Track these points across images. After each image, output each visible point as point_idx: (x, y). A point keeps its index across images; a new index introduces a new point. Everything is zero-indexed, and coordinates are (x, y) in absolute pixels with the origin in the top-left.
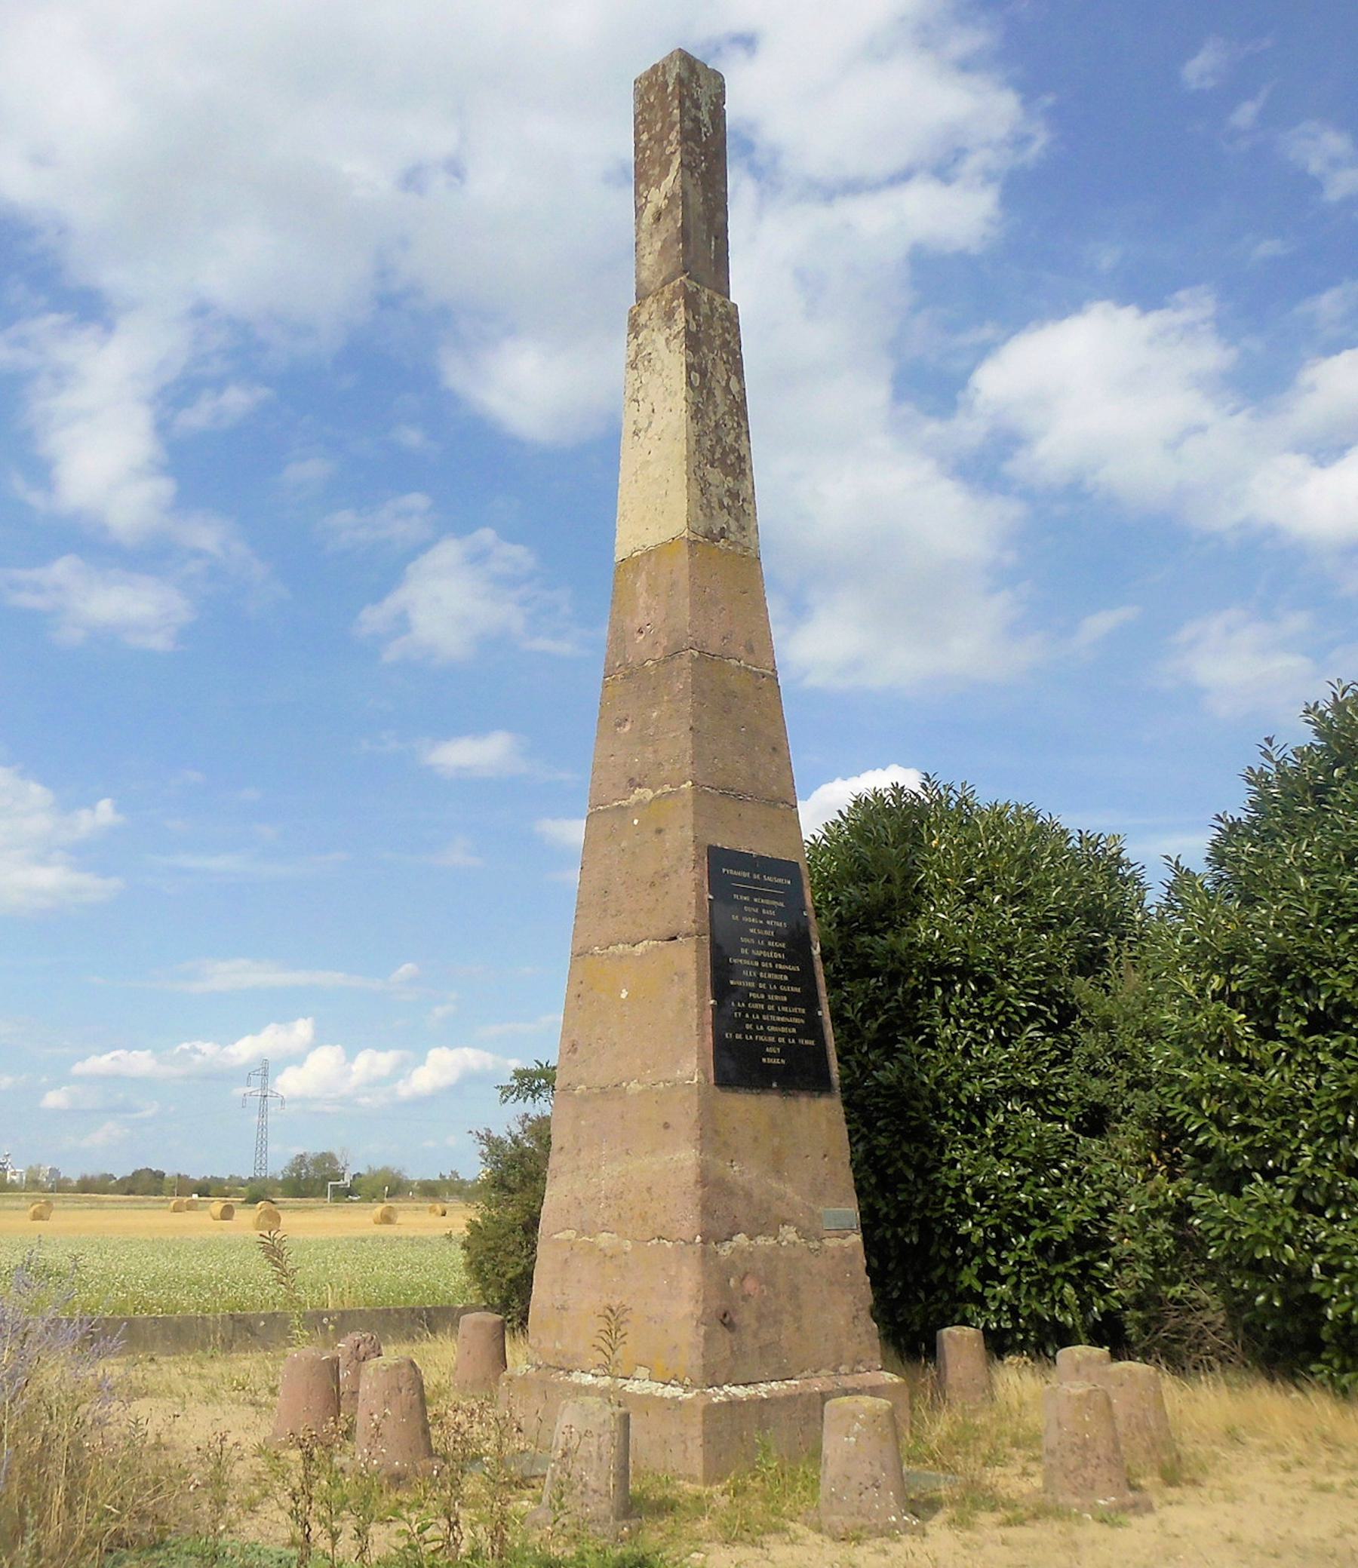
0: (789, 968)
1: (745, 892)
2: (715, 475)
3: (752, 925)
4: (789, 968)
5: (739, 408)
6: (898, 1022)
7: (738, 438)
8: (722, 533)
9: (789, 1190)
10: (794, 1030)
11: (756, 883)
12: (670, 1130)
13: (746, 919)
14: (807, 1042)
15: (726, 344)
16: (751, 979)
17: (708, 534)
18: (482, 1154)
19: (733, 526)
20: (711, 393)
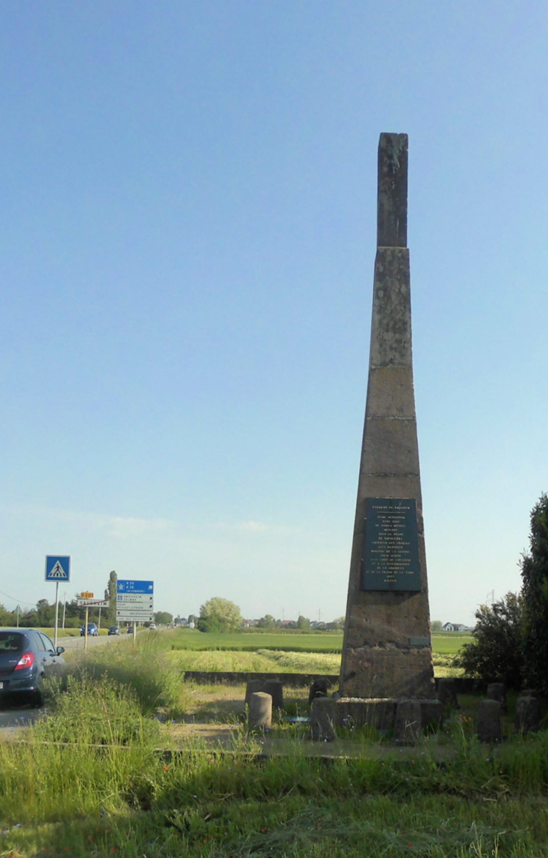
0: (403, 543)
1: (383, 515)
2: (389, 336)
3: (386, 528)
4: (403, 543)
5: (406, 300)
6: (56, 674)
7: (404, 314)
8: (391, 361)
9: (394, 630)
10: (403, 568)
11: (391, 510)
12: (46, 659)
13: (383, 526)
14: (409, 573)
15: (400, 270)
16: (382, 549)
17: (384, 364)
18: (173, 723)
19: (397, 355)
20: (389, 298)
